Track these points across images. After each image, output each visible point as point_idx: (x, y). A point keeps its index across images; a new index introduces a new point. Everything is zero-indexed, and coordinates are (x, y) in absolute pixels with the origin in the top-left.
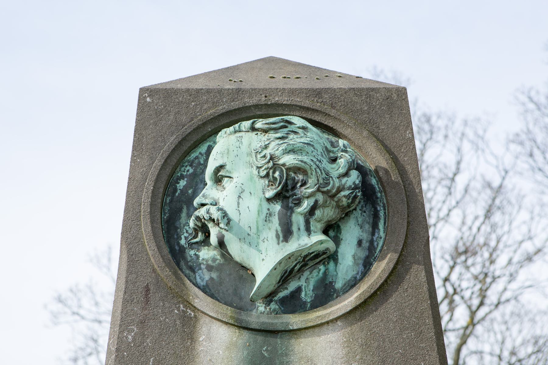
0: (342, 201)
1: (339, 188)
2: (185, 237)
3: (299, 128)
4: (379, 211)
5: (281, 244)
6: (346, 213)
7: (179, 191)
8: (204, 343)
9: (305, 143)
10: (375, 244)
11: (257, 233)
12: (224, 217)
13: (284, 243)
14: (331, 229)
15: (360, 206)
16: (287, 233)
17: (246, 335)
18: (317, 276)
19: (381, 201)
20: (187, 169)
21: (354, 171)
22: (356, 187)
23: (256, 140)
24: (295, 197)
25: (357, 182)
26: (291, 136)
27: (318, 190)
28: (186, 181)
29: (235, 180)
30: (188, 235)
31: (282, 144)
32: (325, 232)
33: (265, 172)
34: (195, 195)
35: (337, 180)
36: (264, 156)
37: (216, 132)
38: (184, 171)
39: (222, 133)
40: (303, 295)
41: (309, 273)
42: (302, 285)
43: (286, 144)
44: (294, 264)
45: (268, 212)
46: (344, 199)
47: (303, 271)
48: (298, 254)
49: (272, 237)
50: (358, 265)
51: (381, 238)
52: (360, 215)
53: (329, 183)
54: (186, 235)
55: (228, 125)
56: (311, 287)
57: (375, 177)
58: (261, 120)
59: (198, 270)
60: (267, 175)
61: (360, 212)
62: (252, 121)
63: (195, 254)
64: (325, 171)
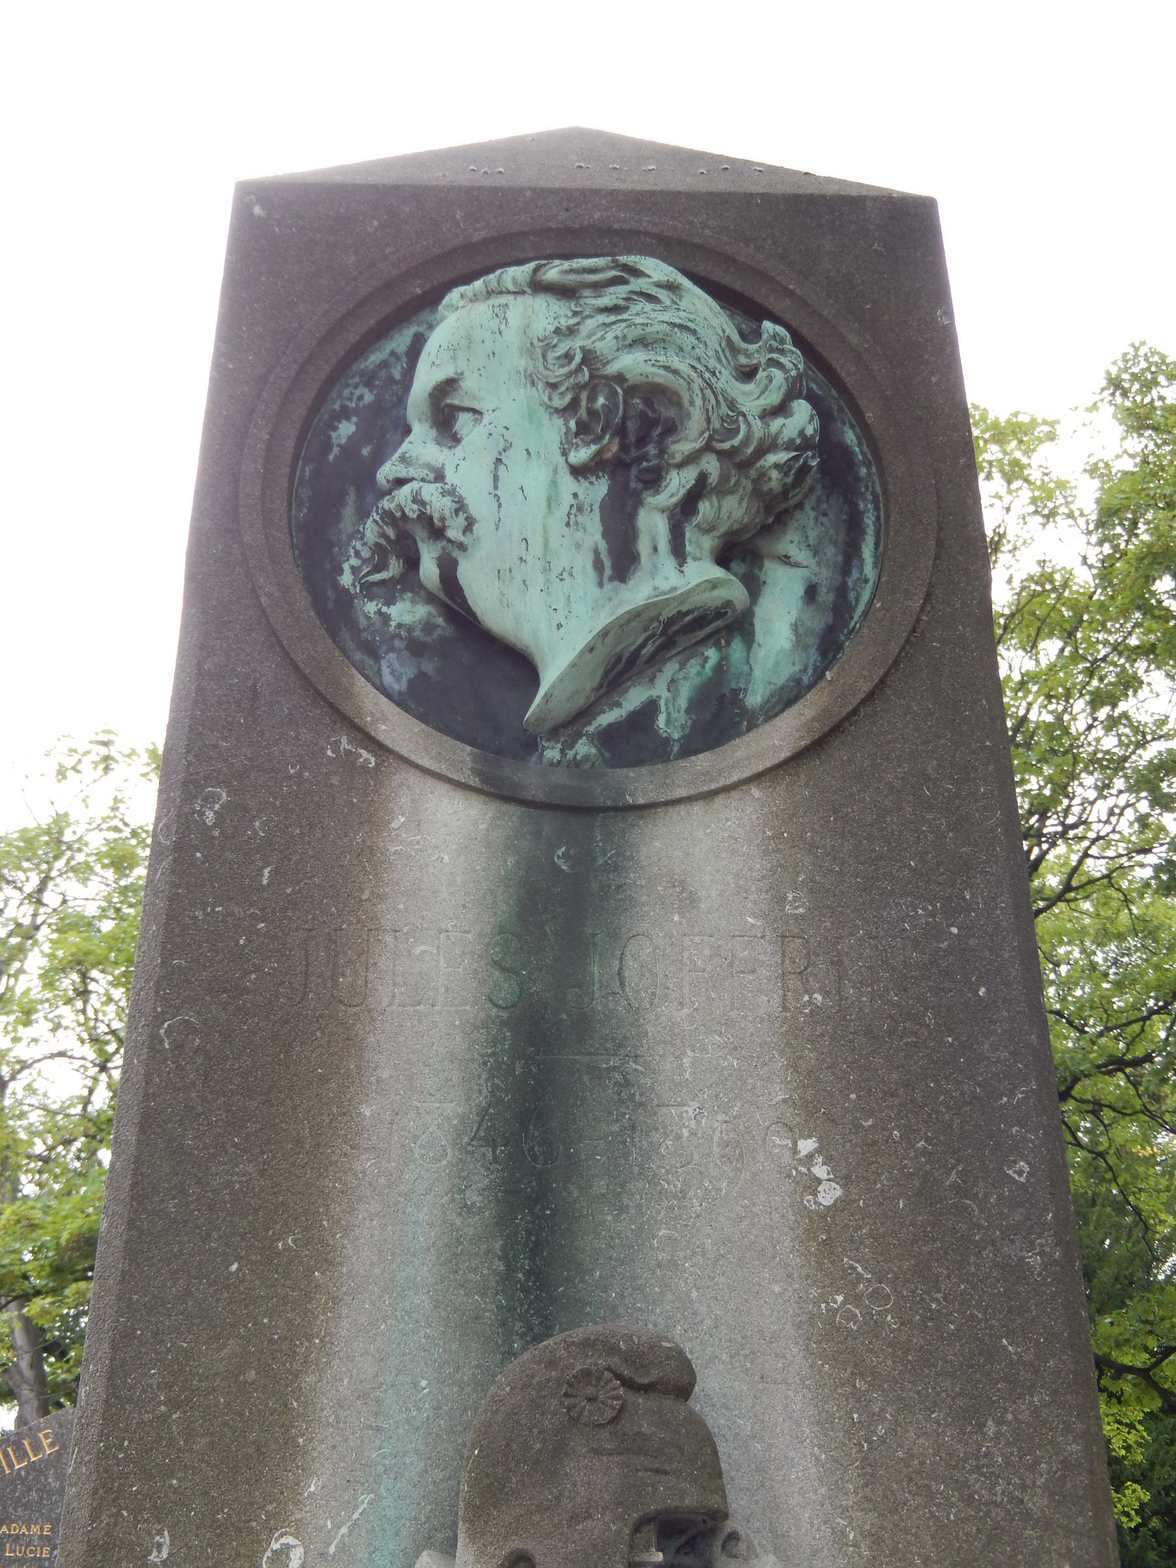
0: (770, 479)
1: (761, 441)
2: (352, 568)
3: (658, 285)
4: (863, 513)
5: (608, 586)
6: (775, 513)
7: (336, 450)
8: (404, 835)
9: (674, 325)
10: (852, 595)
11: (545, 555)
12: (457, 511)
13: (616, 583)
14: (739, 552)
15: (814, 499)
16: (621, 559)
17: (513, 809)
18: (699, 674)
19: (867, 487)
20: (358, 392)
21: (802, 402)
22: (803, 444)
23: (545, 314)
24: (645, 464)
25: (810, 431)
26: (642, 305)
27: (708, 448)
28: (357, 424)
29: (486, 419)
30: (359, 562)
31: (614, 323)
32: (723, 559)
33: (568, 398)
34: (379, 458)
35: (759, 422)
36: (568, 357)
37: (432, 298)
38: (350, 399)
39: (454, 295)
40: (661, 721)
41: (677, 666)
42: (659, 697)
43: (623, 325)
44: (640, 641)
45: (574, 502)
46: (775, 474)
47: (664, 661)
48: (652, 614)
49: (584, 567)
50: (805, 648)
51: (866, 581)
52: (812, 522)
53: (738, 430)
54: (354, 561)
55: (467, 279)
56: (683, 702)
57: (852, 427)
58: (557, 262)
59: (387, 653)
60: (574, 405)
61: (812, 514)
62: (532, 265)
63: (379, 612)
64: (725, 399)
